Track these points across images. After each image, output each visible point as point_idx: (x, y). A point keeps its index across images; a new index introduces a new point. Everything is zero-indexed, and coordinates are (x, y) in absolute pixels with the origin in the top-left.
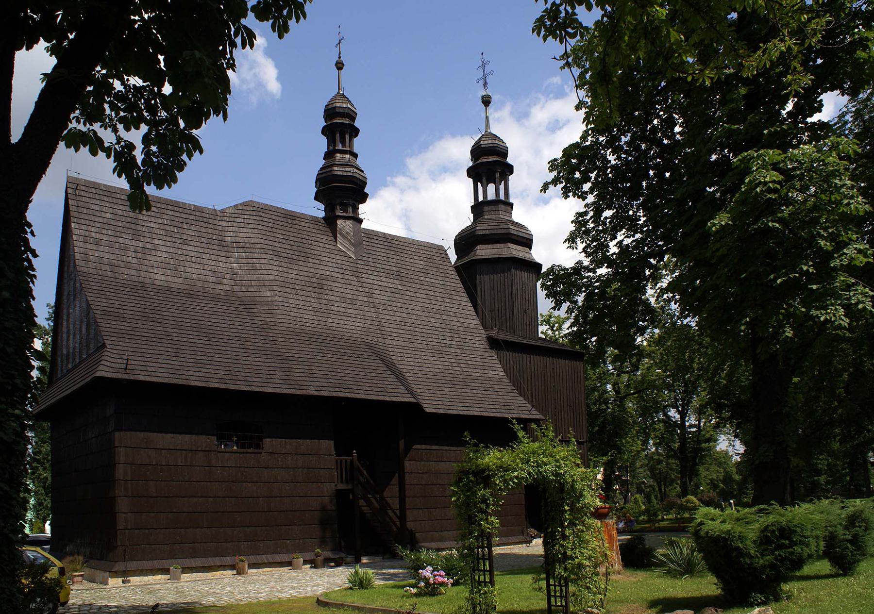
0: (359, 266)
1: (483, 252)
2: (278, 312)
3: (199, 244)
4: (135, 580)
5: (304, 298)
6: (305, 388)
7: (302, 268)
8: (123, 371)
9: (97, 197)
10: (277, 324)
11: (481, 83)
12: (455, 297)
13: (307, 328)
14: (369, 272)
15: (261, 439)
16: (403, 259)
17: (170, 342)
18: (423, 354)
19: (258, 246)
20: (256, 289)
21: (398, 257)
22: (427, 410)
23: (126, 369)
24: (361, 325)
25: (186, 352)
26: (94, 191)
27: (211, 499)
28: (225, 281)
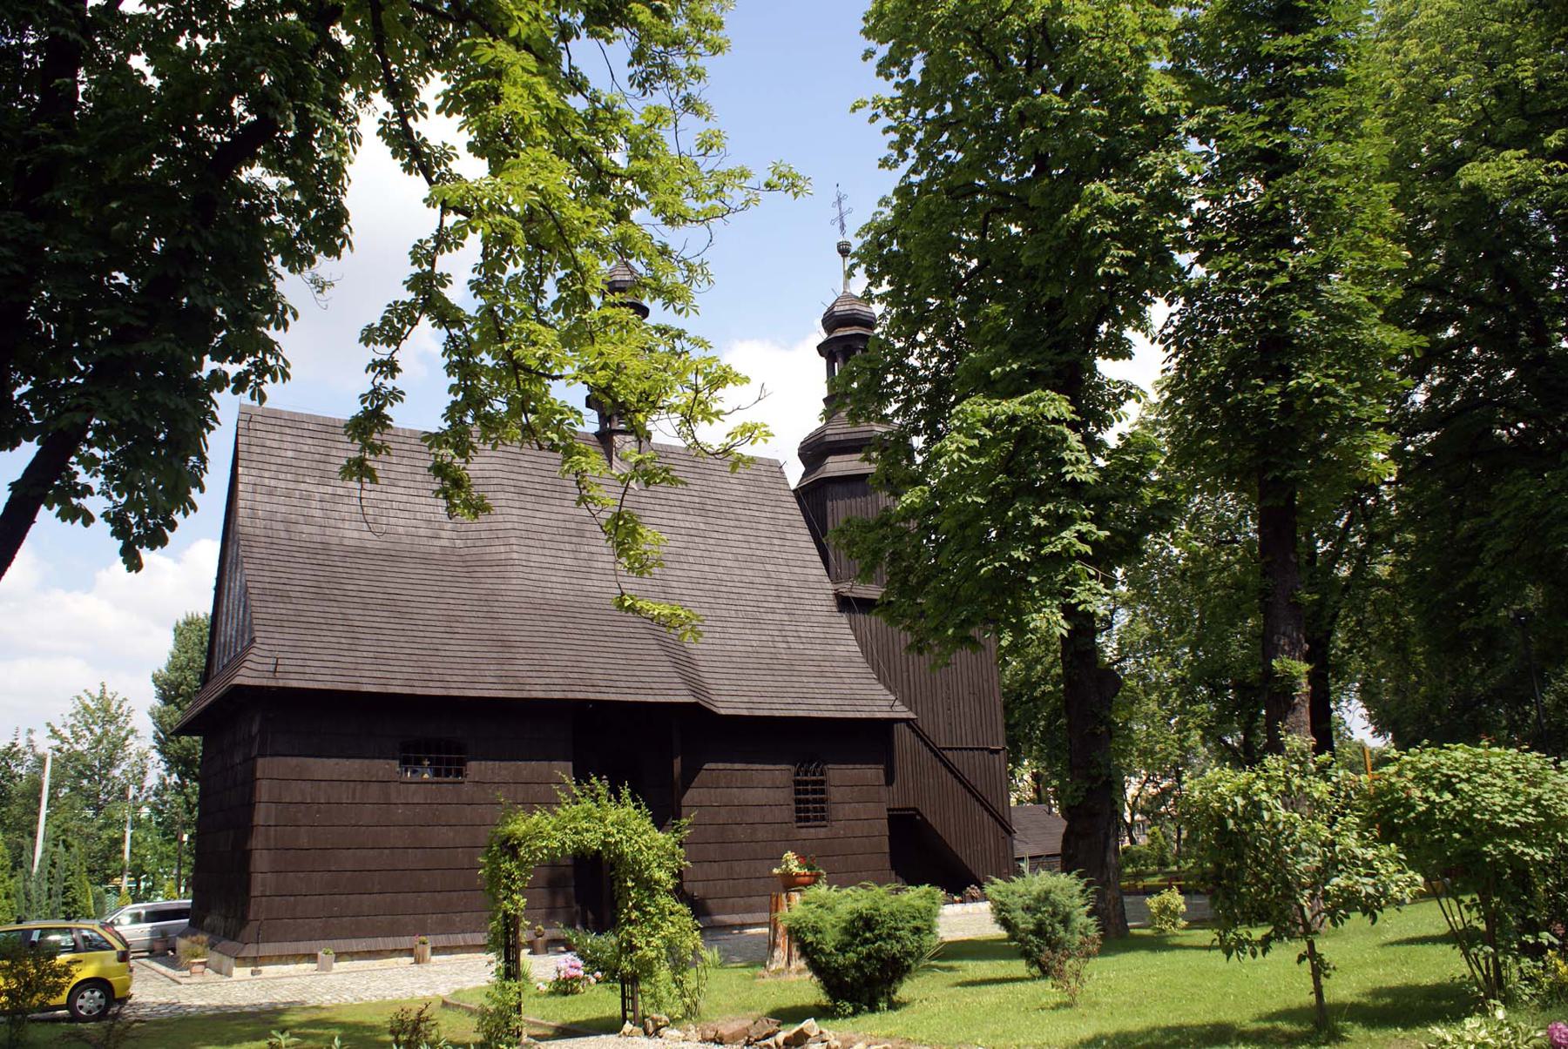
0: (643, 500)
1: (837, 466)
2: (512, 575)
3: (412, 484)
4: (269, 970)
5: (553, 552)
6: (528, 687)
7: (555, 509)
8: (271, 675)
9: (277, 429)
10: (509, 593)
11: (838, 224)
12: (789, 536)
13: (552, 596)
14: (657, 507)
15: (462, 762)
16: (712, 484)
17: (346, 628)
18: (729, 624)
19: (495, 481)
20: (486, 542)
21: (704, 483)
22: (723, 712)
23: (275, 671)
24: (637, 587)
25: (366, 642)
26: (273, 421)
27: (387, 851)
28: (443, 534)
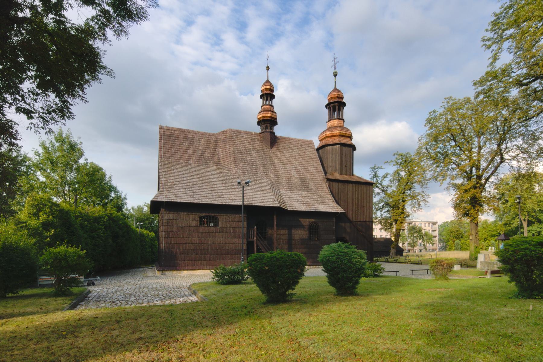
11: (333, 67)
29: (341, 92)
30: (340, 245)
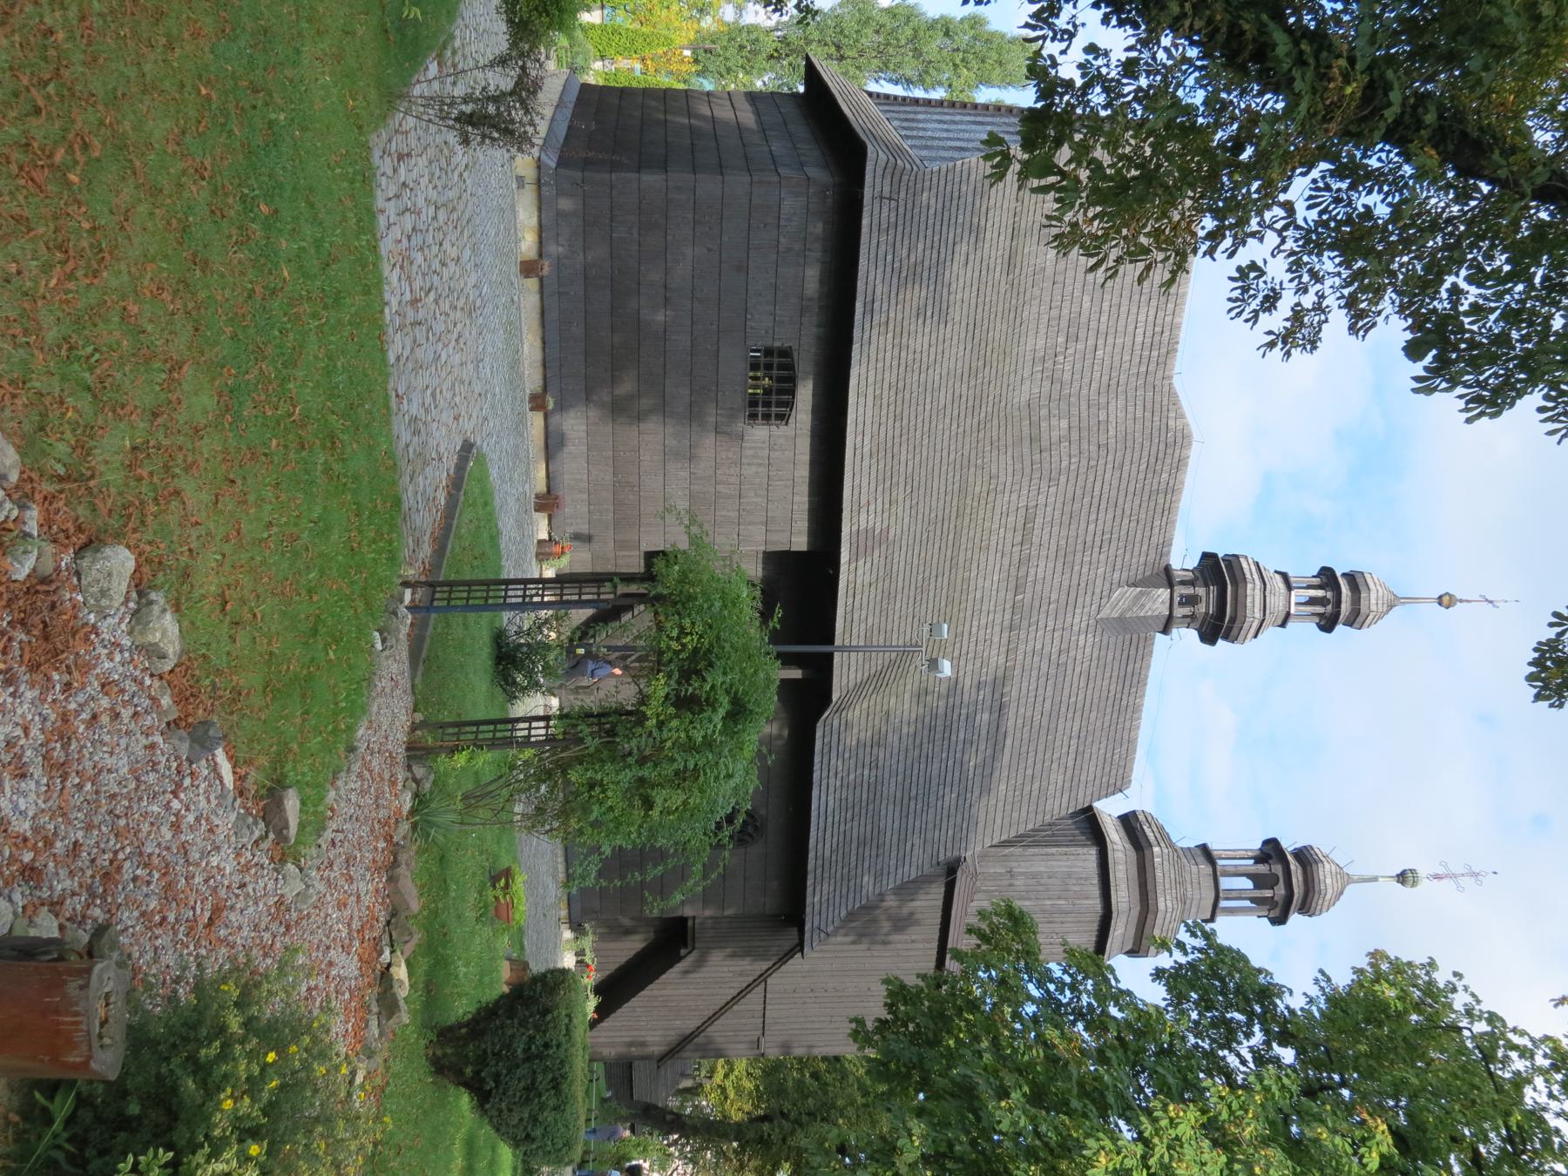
11: (1441, 870)
29: (1333, 903)
30: (24, 335)
